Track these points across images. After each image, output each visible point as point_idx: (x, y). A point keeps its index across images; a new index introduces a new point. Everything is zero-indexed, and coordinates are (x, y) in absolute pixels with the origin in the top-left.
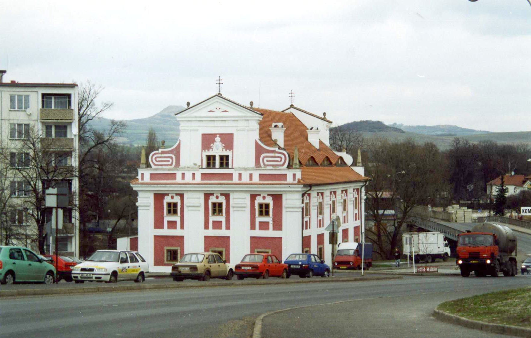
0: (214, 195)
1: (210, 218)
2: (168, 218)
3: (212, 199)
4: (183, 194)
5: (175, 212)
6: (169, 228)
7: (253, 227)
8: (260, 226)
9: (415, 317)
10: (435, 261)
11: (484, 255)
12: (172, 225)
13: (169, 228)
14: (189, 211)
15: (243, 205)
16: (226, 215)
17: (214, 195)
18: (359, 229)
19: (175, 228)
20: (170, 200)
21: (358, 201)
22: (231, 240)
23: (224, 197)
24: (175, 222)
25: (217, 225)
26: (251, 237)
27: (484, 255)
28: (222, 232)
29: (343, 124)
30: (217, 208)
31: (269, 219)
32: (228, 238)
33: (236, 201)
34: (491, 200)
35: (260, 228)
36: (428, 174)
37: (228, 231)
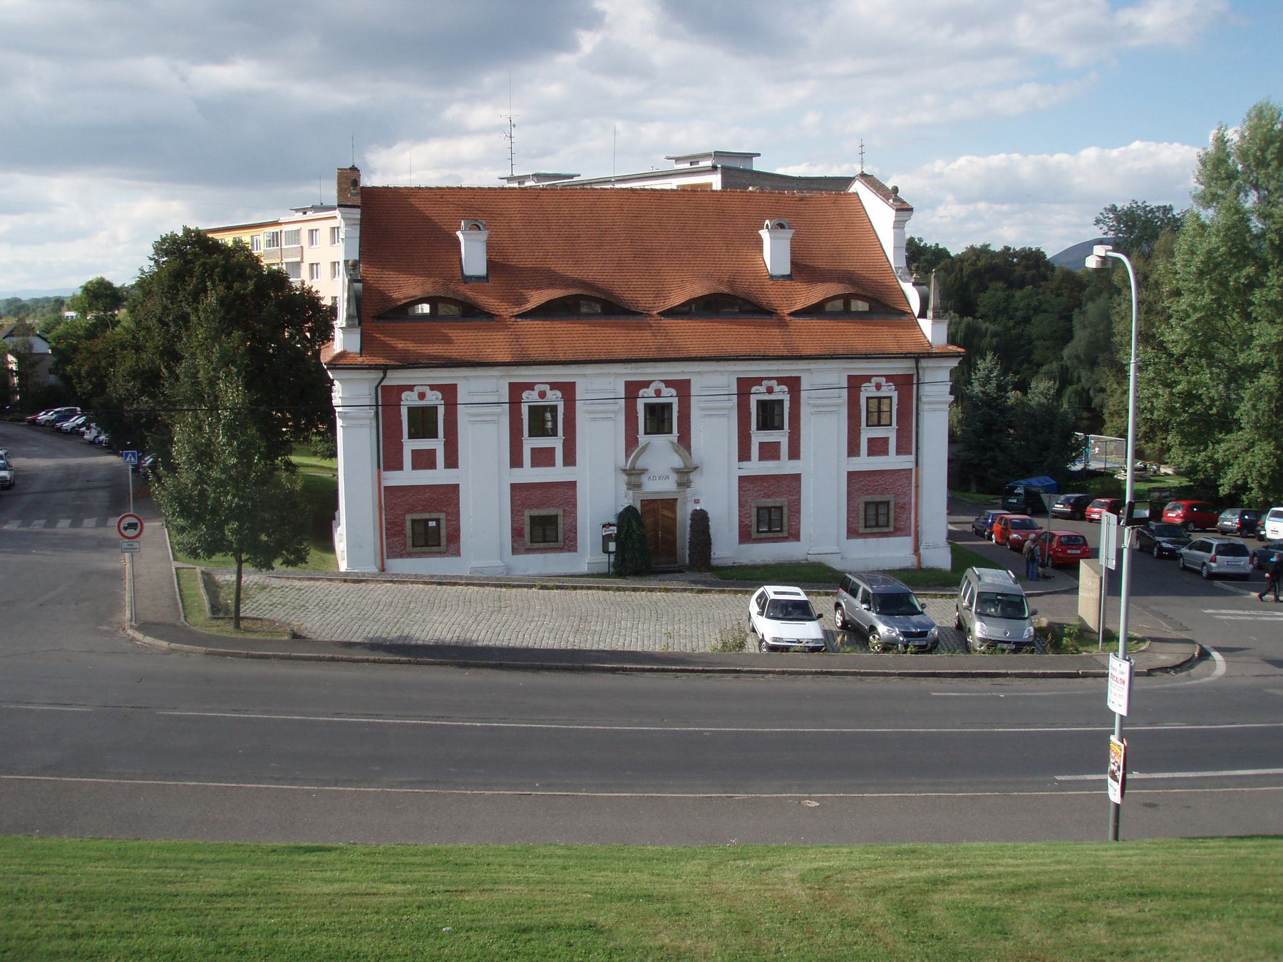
0: (533, 390)
4: (798, 379)
6: (415, 467)
9: (1162, 653)
10: (108, 525)
12: (424, 460)
13: (415, 467)
17: (533, 390)
18: (909, 478)
19: (552, 463)
20: (415, 402)
22: (461, 489)
23: (559, 394)
24: (552, 450)
25: (543, 458)
29: (380, 185)
30: (769, 416)
32: (455, 488)
35: (415, 466)
36: (128, 364)
37: (570, 469)
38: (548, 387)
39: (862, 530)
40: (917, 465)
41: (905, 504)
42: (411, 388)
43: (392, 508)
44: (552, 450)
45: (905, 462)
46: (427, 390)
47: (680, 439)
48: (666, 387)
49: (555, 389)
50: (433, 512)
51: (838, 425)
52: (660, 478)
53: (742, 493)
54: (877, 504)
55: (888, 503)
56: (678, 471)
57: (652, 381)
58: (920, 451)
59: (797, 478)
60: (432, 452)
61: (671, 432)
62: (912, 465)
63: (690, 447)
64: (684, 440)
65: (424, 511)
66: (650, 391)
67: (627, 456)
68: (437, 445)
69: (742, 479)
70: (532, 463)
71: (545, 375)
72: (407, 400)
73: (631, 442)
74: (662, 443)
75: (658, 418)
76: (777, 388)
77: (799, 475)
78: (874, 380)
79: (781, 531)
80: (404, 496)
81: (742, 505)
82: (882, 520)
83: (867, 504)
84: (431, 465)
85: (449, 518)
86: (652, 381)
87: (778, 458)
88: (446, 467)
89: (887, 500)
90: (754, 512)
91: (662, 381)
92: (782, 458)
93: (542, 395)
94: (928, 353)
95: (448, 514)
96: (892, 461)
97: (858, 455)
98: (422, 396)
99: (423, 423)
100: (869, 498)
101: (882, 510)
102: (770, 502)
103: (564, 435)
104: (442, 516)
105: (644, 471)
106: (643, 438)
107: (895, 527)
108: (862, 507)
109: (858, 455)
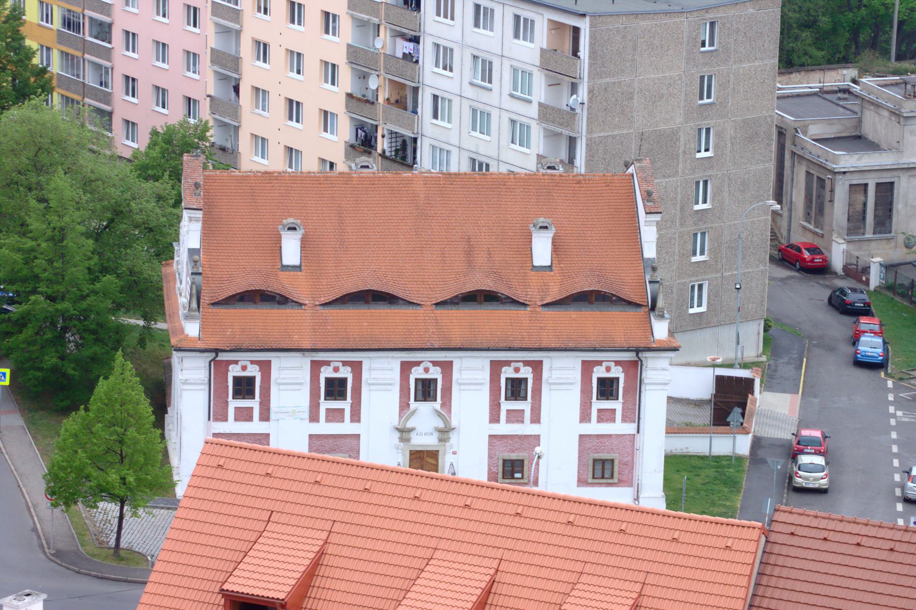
1: (593, 404)
3: (417, 373)
5: (250, 394)
7: (494, 418)
8: (599, 417)
12: (244, 415)
14: (552, 392)
15: (569, 381)
16: (260, 398)
19: (613, 420)
25: (515, 417)
26: (311, 436)
28: (526, 428)
31: (617, 405)
33: (375, 374)
35: (509, 421)
37: (356, 425)
38: (341, 364)
39: (590, 480)
40: (638, 432)
41: (628, 462)
42: (236, 362)
44: (251, 409)
45: (629, 428)
46: (248, 364)
48: (434, 366)
49: (346, 365)
51: (574, 396)
52: (425, 434)
53: (490, 447)
54: (603, 461)
55: (612, 461)
56: (440, 431)
57: (423, 361)
58: (641, 421)
60: (251, 409)
62: (634, 431)
64: (447, 403)
67: (400, 417)
70: (326, 420)
71: (586, 357)
73: (404, 406)
74: (425, 408)
75: (426, 390)
76: (342, 369)
78: (333, 365)
79: (522, 478)
82: (606, 475)
83: (595, 461)
84: (250, 418)
86: (423, 361)
88: (598, 422)
89: (612, 458)
90: (501, 463)
91: (430, 362)
94: (649, 348)
96: (619, 427)
97: (589, 421)
98: (426, 370)
99: (244, 387)
100: (597, 456)
101: (608, 466)
102: (514, 456)
105: (411, 430)
106: (413, 405)
107: (619, 479)
108: (591, 463)
109: (589, 421)
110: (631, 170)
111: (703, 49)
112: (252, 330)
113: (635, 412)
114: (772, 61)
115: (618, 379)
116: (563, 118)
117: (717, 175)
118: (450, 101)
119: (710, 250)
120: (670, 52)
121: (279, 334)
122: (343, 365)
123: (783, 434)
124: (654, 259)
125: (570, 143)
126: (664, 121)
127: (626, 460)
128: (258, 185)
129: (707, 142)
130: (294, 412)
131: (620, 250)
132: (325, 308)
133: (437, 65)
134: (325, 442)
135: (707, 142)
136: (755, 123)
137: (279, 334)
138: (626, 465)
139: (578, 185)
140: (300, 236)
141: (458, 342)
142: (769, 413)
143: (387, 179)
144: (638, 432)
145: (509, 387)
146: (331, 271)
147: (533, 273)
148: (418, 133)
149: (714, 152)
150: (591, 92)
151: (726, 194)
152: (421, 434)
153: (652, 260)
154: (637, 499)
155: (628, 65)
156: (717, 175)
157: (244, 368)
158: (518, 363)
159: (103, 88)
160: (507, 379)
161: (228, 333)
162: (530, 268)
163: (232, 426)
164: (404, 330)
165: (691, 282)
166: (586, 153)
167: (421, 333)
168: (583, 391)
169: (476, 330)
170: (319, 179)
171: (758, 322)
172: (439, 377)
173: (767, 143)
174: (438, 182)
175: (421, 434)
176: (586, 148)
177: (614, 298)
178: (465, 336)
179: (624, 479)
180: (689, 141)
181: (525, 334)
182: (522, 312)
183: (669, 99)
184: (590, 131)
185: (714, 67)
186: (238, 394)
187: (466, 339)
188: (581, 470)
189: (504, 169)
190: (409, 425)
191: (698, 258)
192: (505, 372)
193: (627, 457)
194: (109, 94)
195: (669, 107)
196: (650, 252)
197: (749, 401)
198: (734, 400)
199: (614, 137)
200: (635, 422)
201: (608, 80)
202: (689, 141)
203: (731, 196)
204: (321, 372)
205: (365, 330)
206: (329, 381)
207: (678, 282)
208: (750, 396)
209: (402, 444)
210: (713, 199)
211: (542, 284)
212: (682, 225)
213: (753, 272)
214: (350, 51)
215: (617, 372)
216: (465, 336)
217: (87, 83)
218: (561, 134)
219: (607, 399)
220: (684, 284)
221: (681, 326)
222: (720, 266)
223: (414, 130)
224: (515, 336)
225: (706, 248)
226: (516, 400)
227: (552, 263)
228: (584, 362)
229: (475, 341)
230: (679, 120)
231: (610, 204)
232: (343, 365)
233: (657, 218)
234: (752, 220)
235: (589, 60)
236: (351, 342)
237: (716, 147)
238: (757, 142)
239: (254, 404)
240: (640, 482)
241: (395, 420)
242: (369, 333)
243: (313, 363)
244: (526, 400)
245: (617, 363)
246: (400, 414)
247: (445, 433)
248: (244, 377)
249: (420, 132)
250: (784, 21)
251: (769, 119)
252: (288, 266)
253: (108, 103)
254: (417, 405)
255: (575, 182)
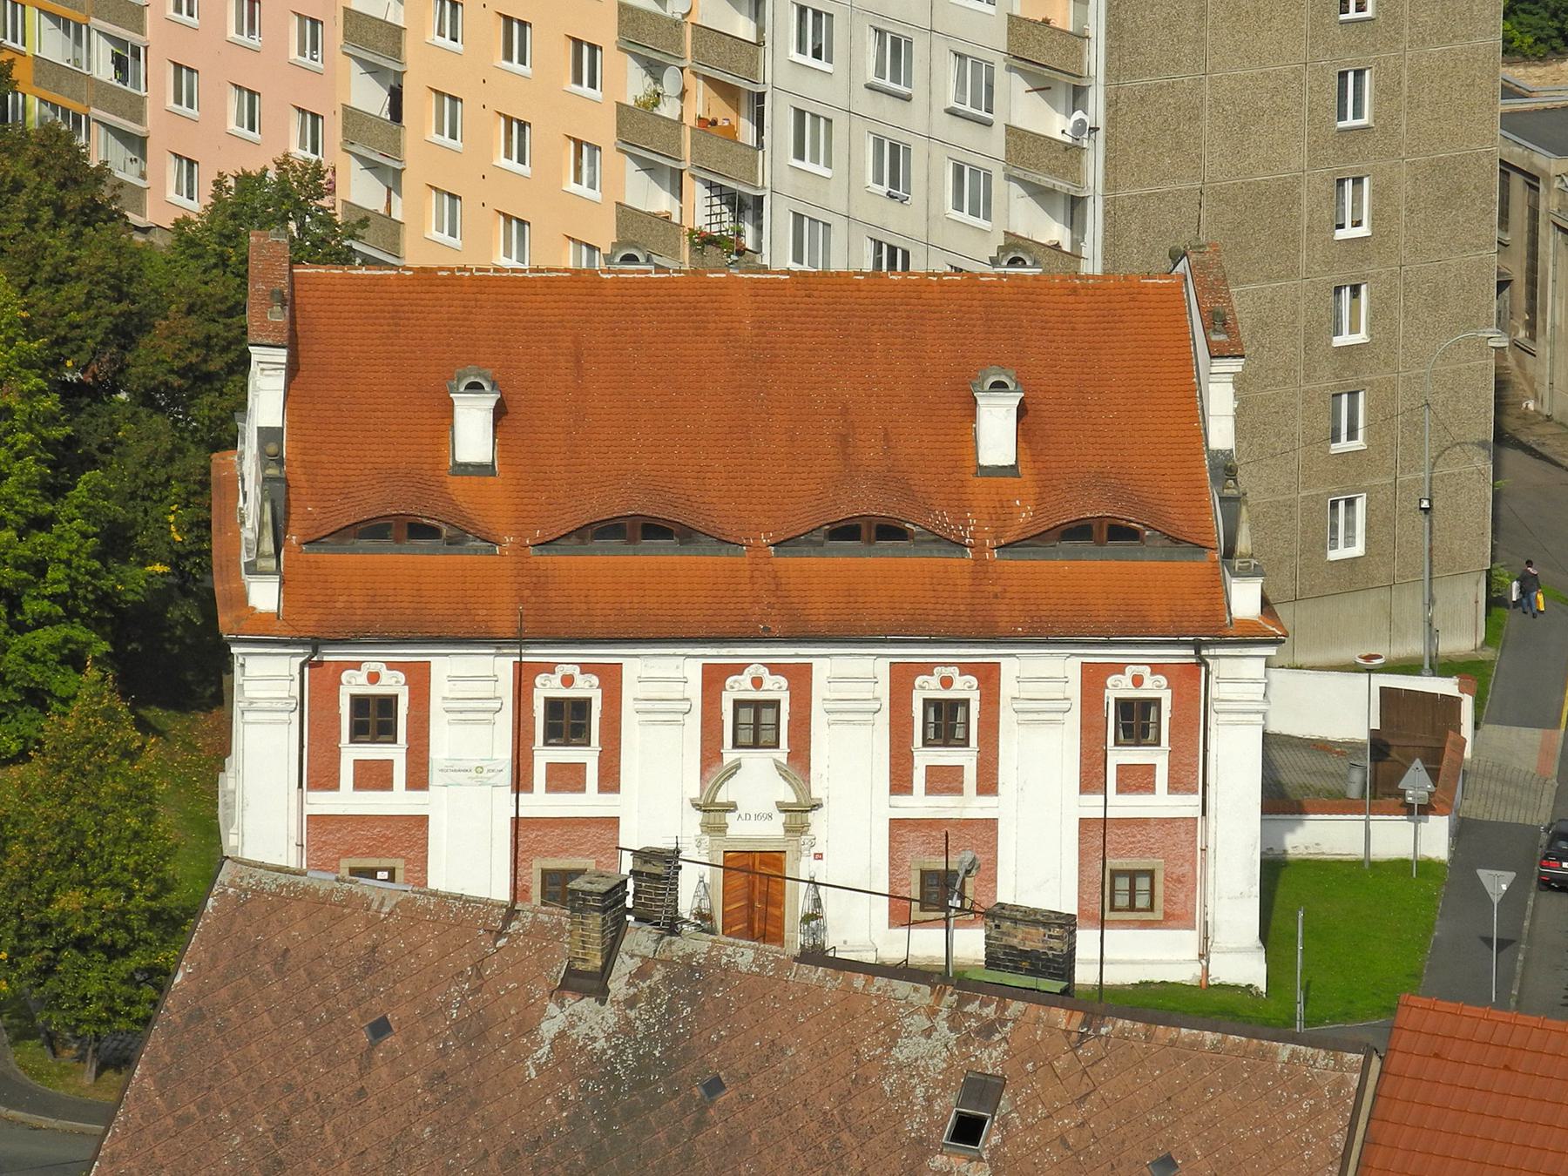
0: (1123, 673)
2: (925, 758)
3: (738, 688)
5: (386, 732)
6: (358, 786)
7: (900, 783)
11: (1540, 597)
12: (374, 777)
13: (358, 786)
17: (1123, 673)
19: (1149, 788)
21: (633, 272)
23: (783, 682)
25: (944, 781)
27: (1540, 597)
31: (1158, 757)
32: (422, 821)
34: (5, 998)
35: (931, 789)
40: (1204, 813)
42: (357, 666)
43: (319, 849)
44: (389, 764)
45: (1185, 806)
47: (790, 756)
48: (772, 673)
50: (384, 856)
54: (1133, 875)
55: (1150, 874)
59: (991, 825)
61: (777, 745)
63: (809, 769)
64: (800, 756)
65: (371, 853)
66: (745, 680)
68: (396, 753)
69: (896, 824)
72: (923, 688)
76: (580, 679)
77: (995, 821)
78: (560, 671)
80: (339, 830)
81: (894, 864)
82: (1142, 901)
84: (385, 784)
85: (410, 867)
87: (958, 791)
92: (965, 790)
93: (757, 683)
95: (408, 861)
96: (1161, 804)
101: (1142, 883)
103: (789, 747)
104: (399, 864)
105: (731, 807)
106: (729, 755)
107: (1165, 913)
110: (1183, 266)
111: (1343, 17)
112: (390, 599)
113: (1197, 771)
114: (1490, 41)
115: (1157, 702)
116: (1056, 158)
117: (1379, 274)
118: (829, 121)
119: (1368, 426)
120: (1276, 23)
121: (448, 606)
122: (582, 673)
123: (1529, 816)
124: (1231, 451)
125: (1072, 214)
126: (1266, 165)
127: (1178, 871)
128: (406, 295)
129: (1357, 207)
130: (479, 769)
131: (1159, 433)
132: (545, 553)
133: (801, 49)
134: (546, 834)
135: (1357, 207)
136: (1456, 168)
137: (448, 606)
138: (1180, 882)
139: (1071, 299)
140: (492, 404)
141: (822, 623)
142: (1495, 770)
143: (674, 285)
144: (1204, 813)
145: (932, 718)
146: (558, 476)
147: (978, 481)
148: (763, 188)
149: (1373, 226)
150: (1112, 104)
151: (1399, 315)
152: (748, 816)
153: (1227, 454)
154: (1204, 955)
155: (1188, 49)
156: (1379, 274)
157: (568, 681)
158: (949, 669)
159: (128, 88)
160: (927, 703)
161: (339, 605)
162: (973, 470)
163: (347, 800)
164: (709, 600)
165: (1330, 494)
166: (1105, 231)
167: (745, 606)
168: (1085, 727)
169: (860, 599)
170: (533, 284)
171: (1475, 577)
172: (974, 698)
173: (1483, 210)
174: (782, 292)
175: (748, 816)
176: (1105, 219)
177: (1147, 533)
178: (836, 611)
179: (1176, 912)
180: (1319, 204)
181: (962, 607)
182: (956, 562)
183: (1276, 118)
184: (1111, 184)
185: (1369, 54)
186: (360, 732)
187: (838, 618)
188: (1085, 893)
189: (940, 265)
190: (722, 797)
191: (1344, 445)
192: (922, 688)
193: (1182, 865)
194: (141, 100)
195: (1277, 135)
196: (1221, 434)
197: (1448, 746)
198: (1418, 742)
199: (1161, 198)
200: (1196, 792)
201: (1146, 80)
202: (1319, 204)
203: (1410, 318)
204: (340, 683)
205: (628, 600)
206: (553, 705)
207: (1304, 493)
208: (1451, 733)
209: (707, 838)
210: (1371, 325)
211: (997, 504)
212: (1308, 377)
213: (1460, 474)
214: (625, 18)
215: (965, 688)
216: (836, 611)
217: (95, 75)
218: (1054, 191)
219: (1138, 744)
220: (1316, 499)
221: (1312, 587)
222: (1390, 462)
223: (756, 181)
224: (941, 612)
225: (1361, 424)
226: (946, 745)
227: (1016, 461)
228: (706, 669)
229: (858, 623)
230: (1301, 160)
231: (1139, 337)
232: (582, 673)
233: (1235, 366)
234: (1453, 367)
235: (1107, 39)
236: (598, 625)
237: (1376, 217)
238: (1461, 206)
239: (396, 753)
240: (1209, 918)
241: (694, 790)
242: (636, 606)
243: (520, 668)
244: (967, 745)
245: (1156, 669)
246: (702, 774)
247: (799, 813)
248: (374, 696)
249: (767, 184)
250: (1120, 25)
251: (1485, 161)
252: (467, 465)
253: (139, 118)
254: (738, 756)
255: (1066, 292)
